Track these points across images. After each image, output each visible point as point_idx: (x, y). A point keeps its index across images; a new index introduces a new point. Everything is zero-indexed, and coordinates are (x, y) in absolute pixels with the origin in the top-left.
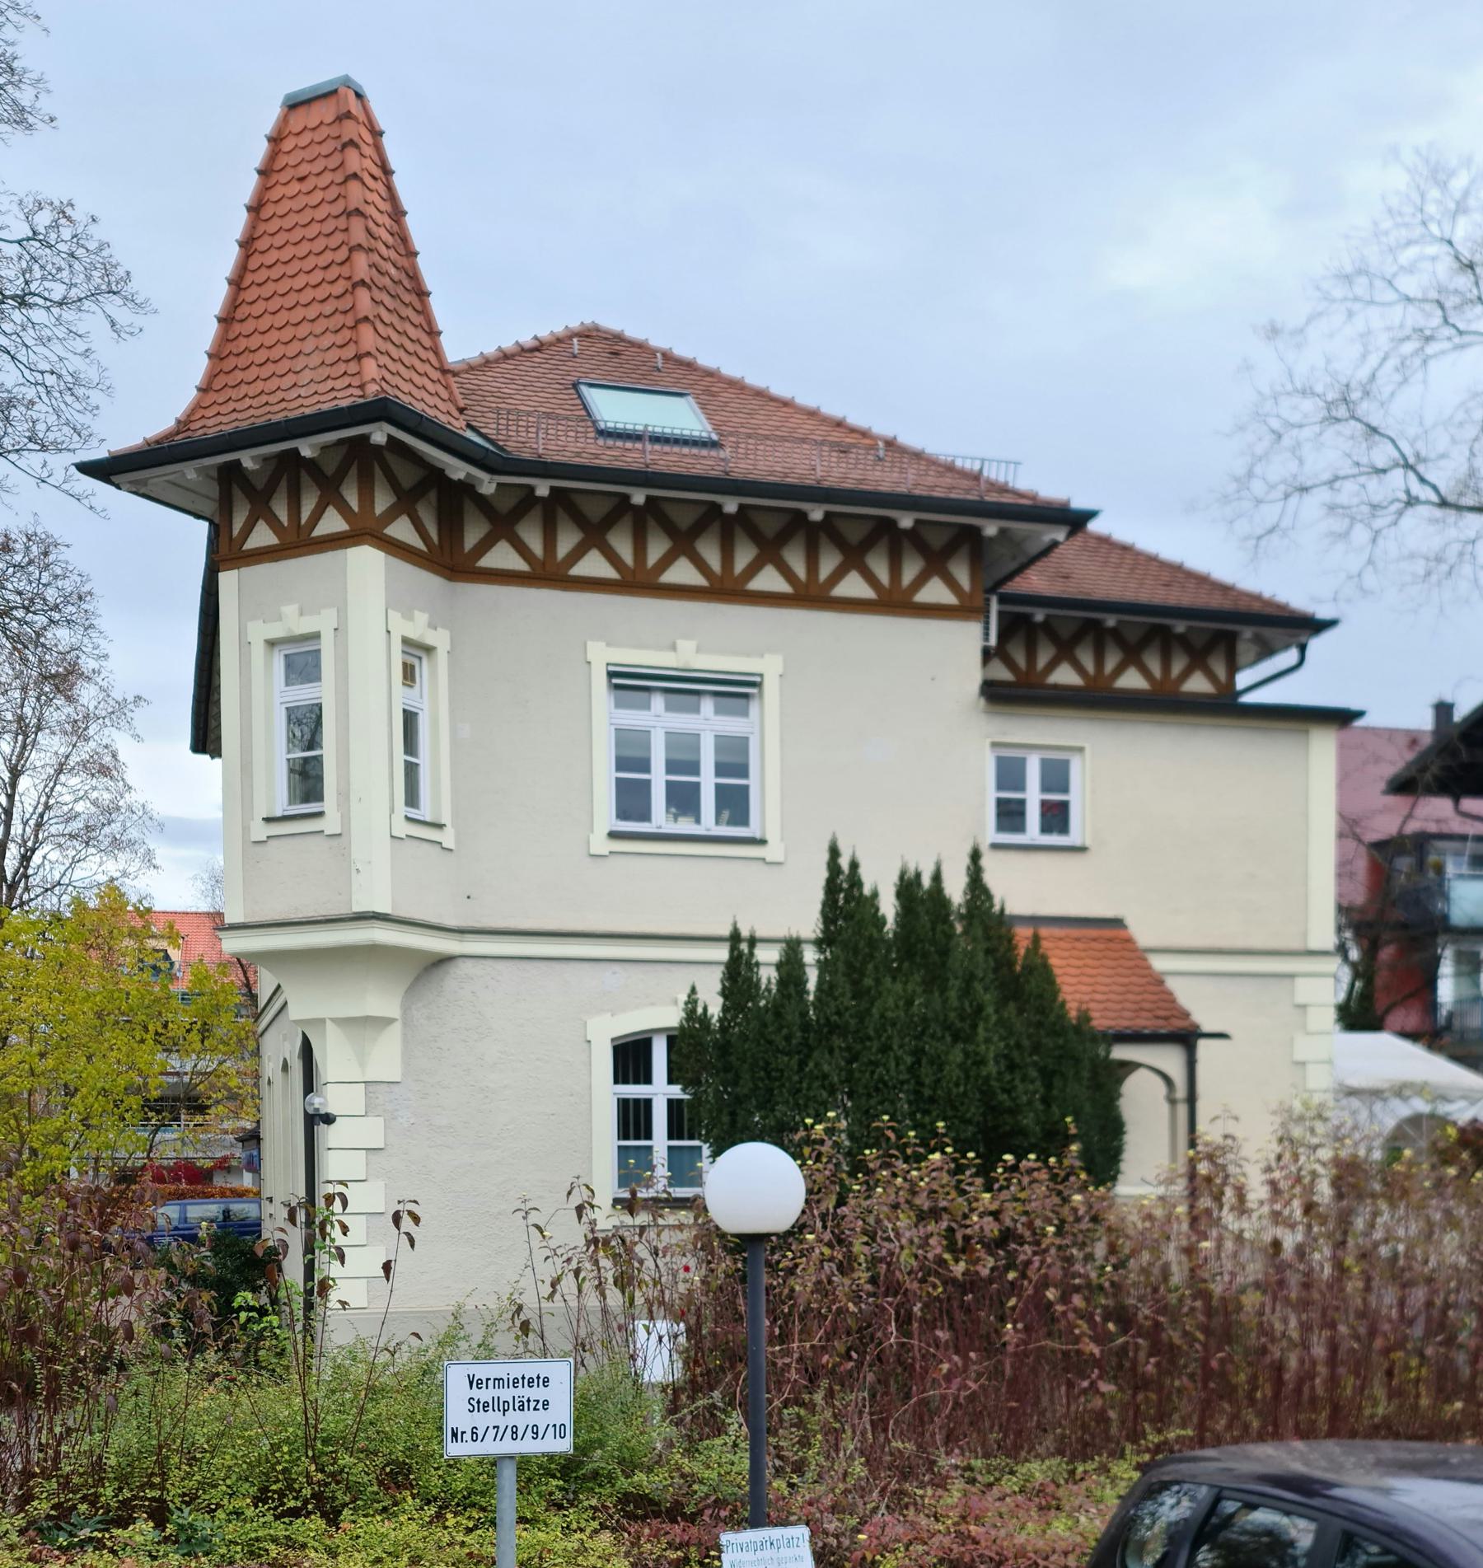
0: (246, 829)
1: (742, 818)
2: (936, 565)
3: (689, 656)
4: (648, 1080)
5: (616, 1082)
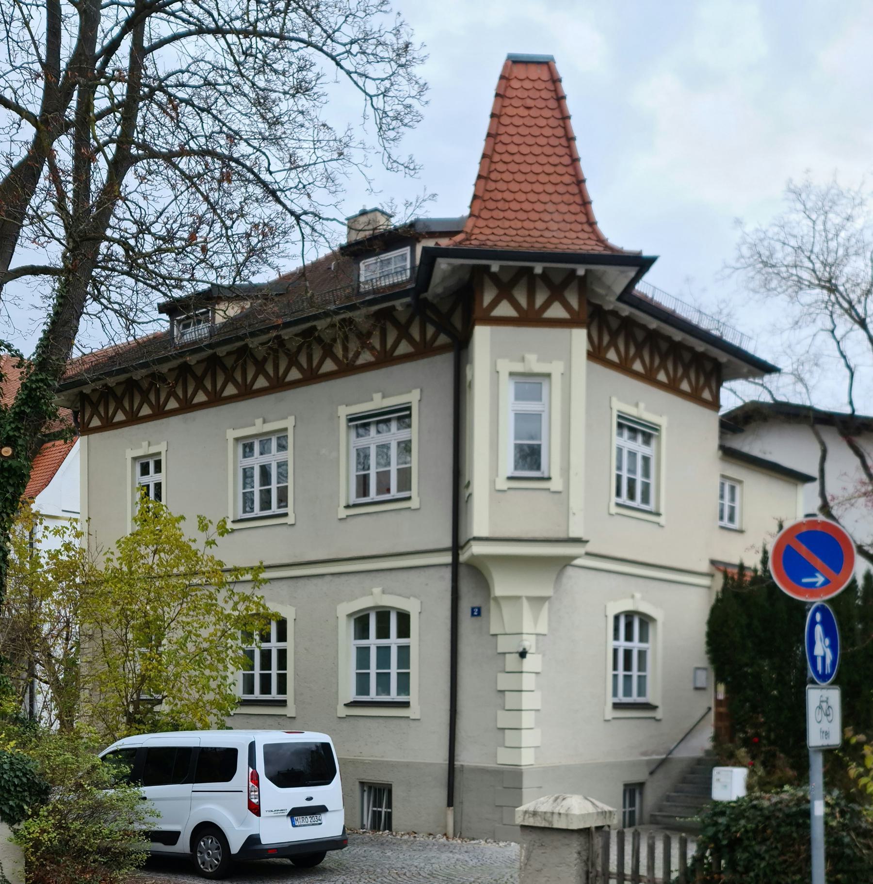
0: (493, 482)
1: (537, 466)
2: (557, 294)
3: (379, 402)
4: (368, 638)
5: (355, 639)
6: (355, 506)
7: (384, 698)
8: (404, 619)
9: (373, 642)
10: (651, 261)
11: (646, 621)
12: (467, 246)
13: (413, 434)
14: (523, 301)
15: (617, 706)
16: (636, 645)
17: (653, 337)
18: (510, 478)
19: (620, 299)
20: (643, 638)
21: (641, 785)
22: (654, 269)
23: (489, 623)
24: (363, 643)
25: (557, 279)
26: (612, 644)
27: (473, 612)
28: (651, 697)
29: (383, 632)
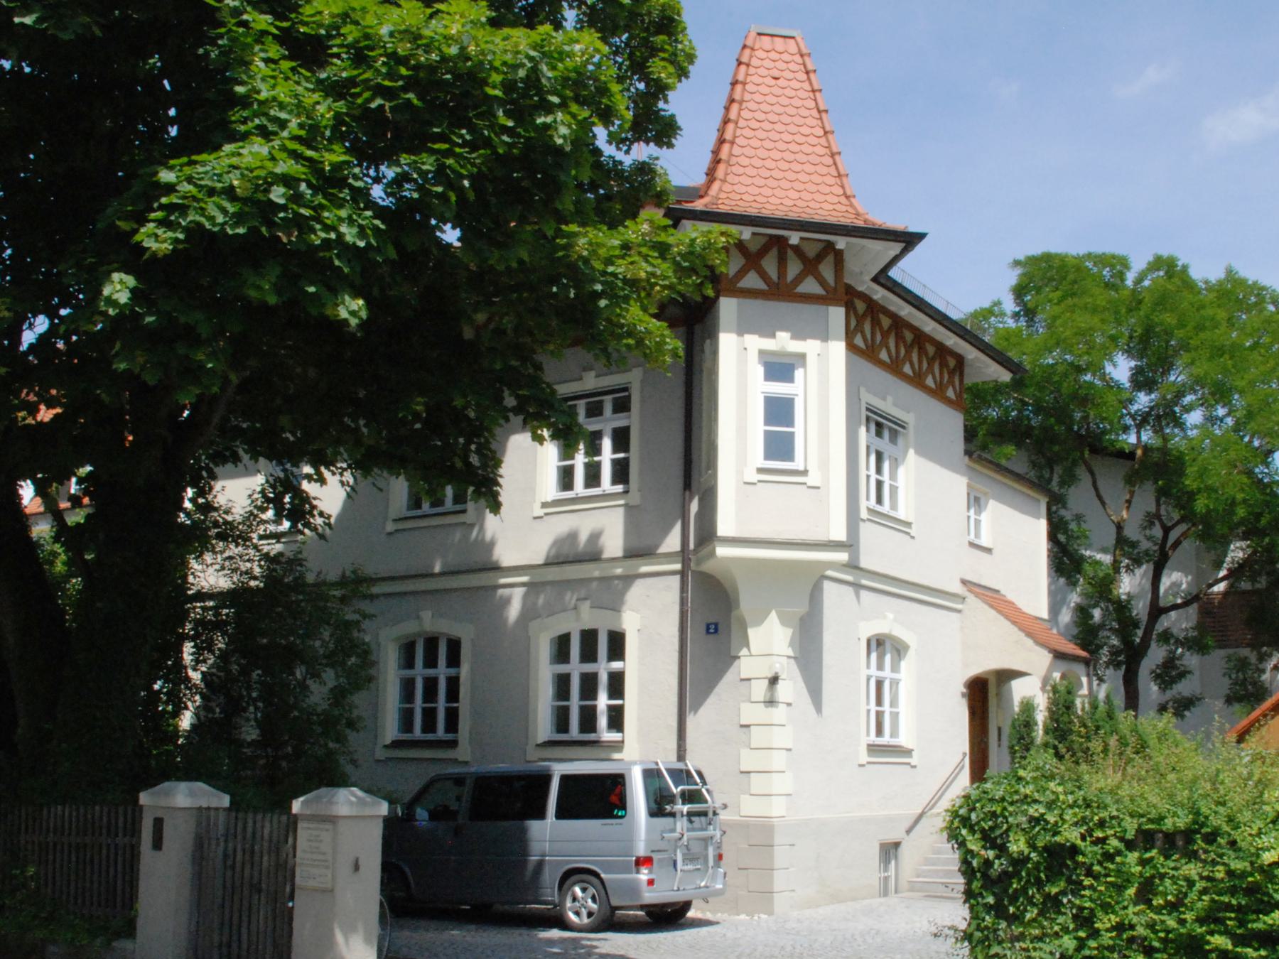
6: (406, 518)
7: (430, 736)
8: (454, 647)
9: (576, 668)
10: (921, 236)
11: (900, 650)
12: (714, 208)
13: (633, 419)
14: (773, 274)
15: (873, 749)
16: (887, 673)
17: (899, 324)
18: (761, 471)
19: (875, 279)
20: (895, 668)
21: (897, 845)
22: (920, 248)
23: (729, 642)
24: (562, 669)
25: (811, 251)
26: (864, 672)
27: (708, 629)
28: (904, 740)
29: (431, 662)
